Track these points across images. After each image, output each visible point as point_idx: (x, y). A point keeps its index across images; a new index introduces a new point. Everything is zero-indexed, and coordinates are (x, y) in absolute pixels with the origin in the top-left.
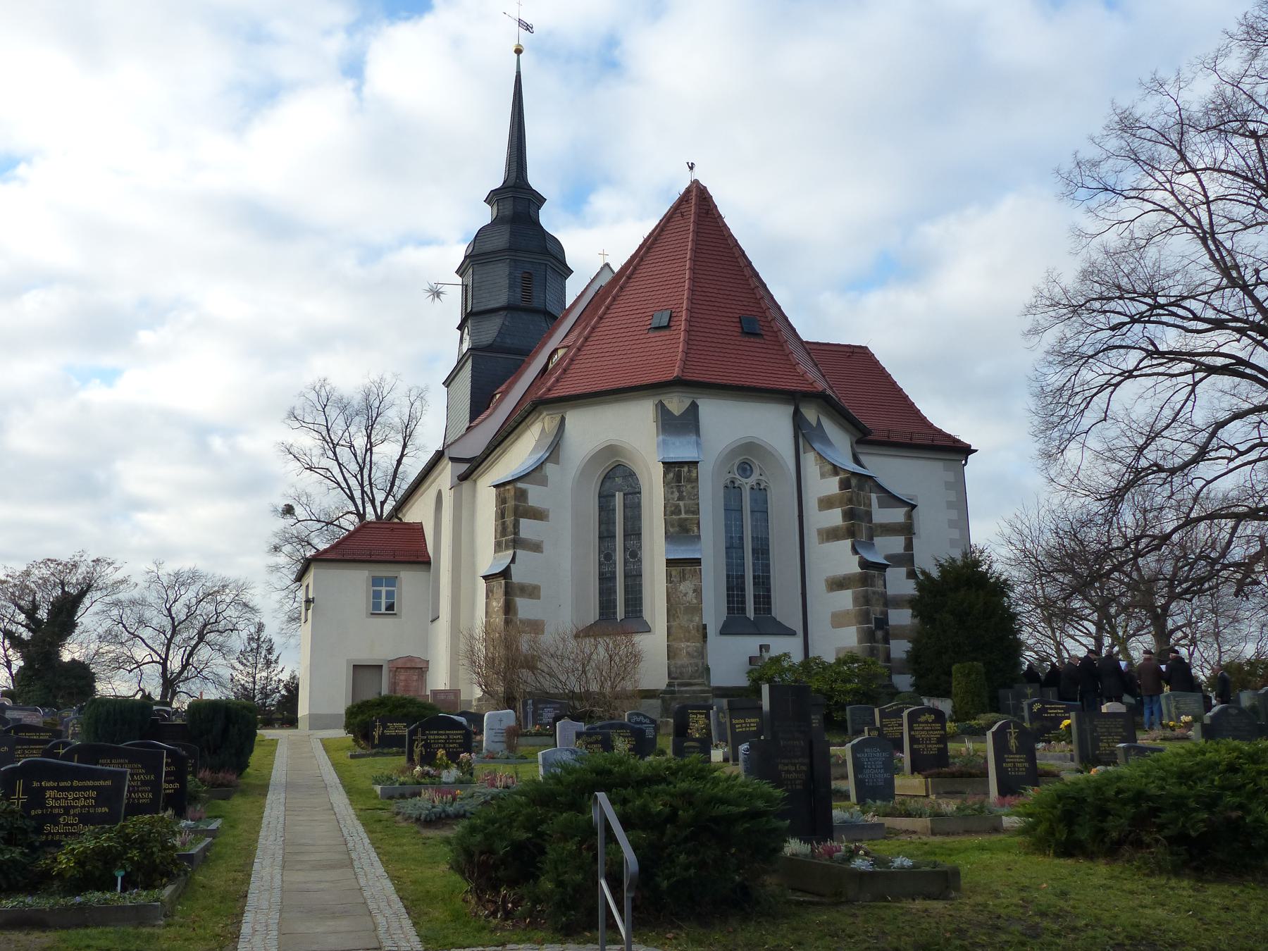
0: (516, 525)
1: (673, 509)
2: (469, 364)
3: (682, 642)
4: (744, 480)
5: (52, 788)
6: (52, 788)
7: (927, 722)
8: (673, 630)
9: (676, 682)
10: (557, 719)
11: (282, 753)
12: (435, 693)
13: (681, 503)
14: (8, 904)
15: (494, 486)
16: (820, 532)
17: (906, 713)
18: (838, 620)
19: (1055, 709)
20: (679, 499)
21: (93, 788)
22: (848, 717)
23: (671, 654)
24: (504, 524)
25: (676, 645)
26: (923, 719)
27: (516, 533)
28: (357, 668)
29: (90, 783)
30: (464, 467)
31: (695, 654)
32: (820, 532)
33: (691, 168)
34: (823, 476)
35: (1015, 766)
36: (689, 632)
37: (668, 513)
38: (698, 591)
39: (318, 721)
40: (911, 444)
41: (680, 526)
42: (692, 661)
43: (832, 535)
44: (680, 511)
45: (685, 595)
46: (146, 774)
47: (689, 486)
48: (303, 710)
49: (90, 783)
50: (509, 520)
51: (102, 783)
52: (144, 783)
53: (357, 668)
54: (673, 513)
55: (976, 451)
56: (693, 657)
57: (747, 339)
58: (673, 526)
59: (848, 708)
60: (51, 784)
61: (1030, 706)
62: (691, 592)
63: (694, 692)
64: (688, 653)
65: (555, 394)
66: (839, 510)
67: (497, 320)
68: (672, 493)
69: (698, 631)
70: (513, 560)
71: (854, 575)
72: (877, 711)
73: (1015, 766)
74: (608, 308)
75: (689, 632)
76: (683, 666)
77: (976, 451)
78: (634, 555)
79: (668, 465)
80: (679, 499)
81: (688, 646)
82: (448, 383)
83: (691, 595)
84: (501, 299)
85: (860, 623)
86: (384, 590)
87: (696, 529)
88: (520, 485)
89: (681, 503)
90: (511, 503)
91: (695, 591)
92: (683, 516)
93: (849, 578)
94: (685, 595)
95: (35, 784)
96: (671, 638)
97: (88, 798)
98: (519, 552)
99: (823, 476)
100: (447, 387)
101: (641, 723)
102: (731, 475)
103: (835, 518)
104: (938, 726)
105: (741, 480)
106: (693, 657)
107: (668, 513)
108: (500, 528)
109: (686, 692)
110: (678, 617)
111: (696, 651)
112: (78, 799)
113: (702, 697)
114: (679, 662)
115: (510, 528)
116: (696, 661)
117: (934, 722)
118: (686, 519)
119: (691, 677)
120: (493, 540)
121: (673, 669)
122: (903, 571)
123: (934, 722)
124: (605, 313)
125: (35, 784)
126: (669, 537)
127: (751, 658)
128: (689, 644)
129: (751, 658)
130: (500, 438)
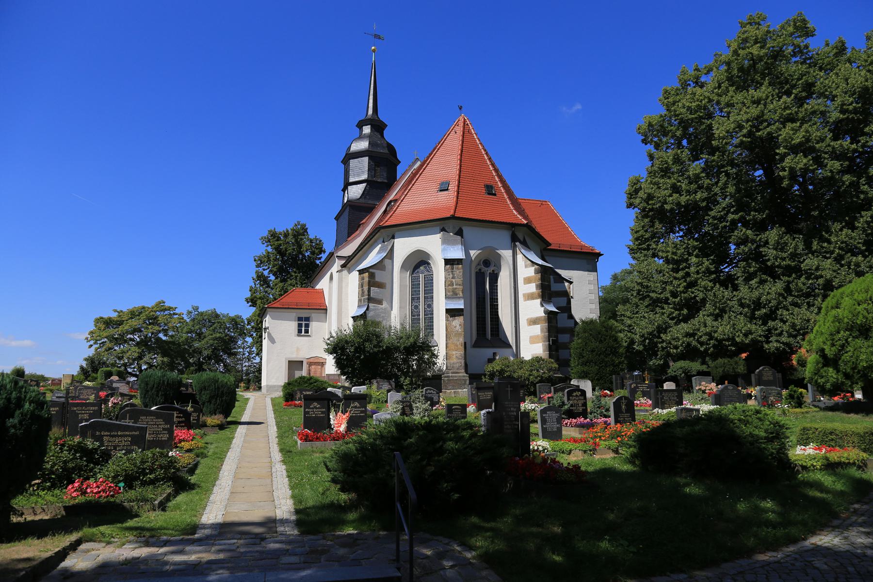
0: (369, 291)
2: (347, 210)
4: (486, 269)
5: (107, 436)
6: (107, 436)
7: (577, 396)
8: (449, 345)
9: (450, 371)
10: (389, 391)
11: (250, 404)
12: (328, 375)
14: (859, 538)
17: (566, 390)
18: (533, 340)
19: (643, 386)
20: (453, 278)
21: (129, 436)
23: (448, 358)
24: (363, 290)
25: (450, 352)
26: (574, 394)
27: (369, 295)
28: (289, 362)
29: (127, 433)
32: (524, 295)
33: (460, 109)
34: (526, 266)
35: (624, 420)
37: (447, 285)
39: (270, 388)
40: (559, 250)
42: (458, 361)
43: (530, 297)
45: (455, 327)
46: (166, 424)
47: (458, 271)
48: (264, 383)
49: (127, 433)
50: (366, 288)
51: (134, 433)
52: (164, 429)
53: (289, 362)
54: (449, 285)
55: (603, 255)
57: (488, 196)
58: (449, 292)
59: (537, 385)
60: (106, 433)
61: (631, 385)
63: (460, 376)
65: (387, 224)
66: (541, 344)
68: (449, 275)
70: (367, 309)
72: (552, 388)
73: (624, 420)
76: (454, 363)
77: (603, 255)
78: (429, 307)
79: (448, 262)
80: (453, 278)
81: (457, 354)
82: (337, 218)
84: (365, 176)
85: (544, 342)
86: (304, 323)
88: (371, 270)
89: (454, 280)
90: (366, 279)
92: (455, 287)
94: (455, 327)
95: (98, 433)
96: (448, 349)
97: (126, 441)
98: (370, 305)
99: (526, 266)
100: (337, 220)
101: (431, 393)
102: (479, 267)
103: (532, 288)
104: (582, 398)
105: (484, 269)
106: (459, 359)
107: (447, 285)
108: (361, 292)
109: (456, 377)
112: (121, 441)
114: (452, 362)
115: (366, 293)
116: (460, 361)
117: (580, 395)
119: (458, 369)
120: (357, 299)
121: (449, 365)
122: (566, 315)
123: (580, 395)
125: (98, 433)
126: (447, 297)
127: (488, 359)
129: (488, 359)
130: (362, 246)
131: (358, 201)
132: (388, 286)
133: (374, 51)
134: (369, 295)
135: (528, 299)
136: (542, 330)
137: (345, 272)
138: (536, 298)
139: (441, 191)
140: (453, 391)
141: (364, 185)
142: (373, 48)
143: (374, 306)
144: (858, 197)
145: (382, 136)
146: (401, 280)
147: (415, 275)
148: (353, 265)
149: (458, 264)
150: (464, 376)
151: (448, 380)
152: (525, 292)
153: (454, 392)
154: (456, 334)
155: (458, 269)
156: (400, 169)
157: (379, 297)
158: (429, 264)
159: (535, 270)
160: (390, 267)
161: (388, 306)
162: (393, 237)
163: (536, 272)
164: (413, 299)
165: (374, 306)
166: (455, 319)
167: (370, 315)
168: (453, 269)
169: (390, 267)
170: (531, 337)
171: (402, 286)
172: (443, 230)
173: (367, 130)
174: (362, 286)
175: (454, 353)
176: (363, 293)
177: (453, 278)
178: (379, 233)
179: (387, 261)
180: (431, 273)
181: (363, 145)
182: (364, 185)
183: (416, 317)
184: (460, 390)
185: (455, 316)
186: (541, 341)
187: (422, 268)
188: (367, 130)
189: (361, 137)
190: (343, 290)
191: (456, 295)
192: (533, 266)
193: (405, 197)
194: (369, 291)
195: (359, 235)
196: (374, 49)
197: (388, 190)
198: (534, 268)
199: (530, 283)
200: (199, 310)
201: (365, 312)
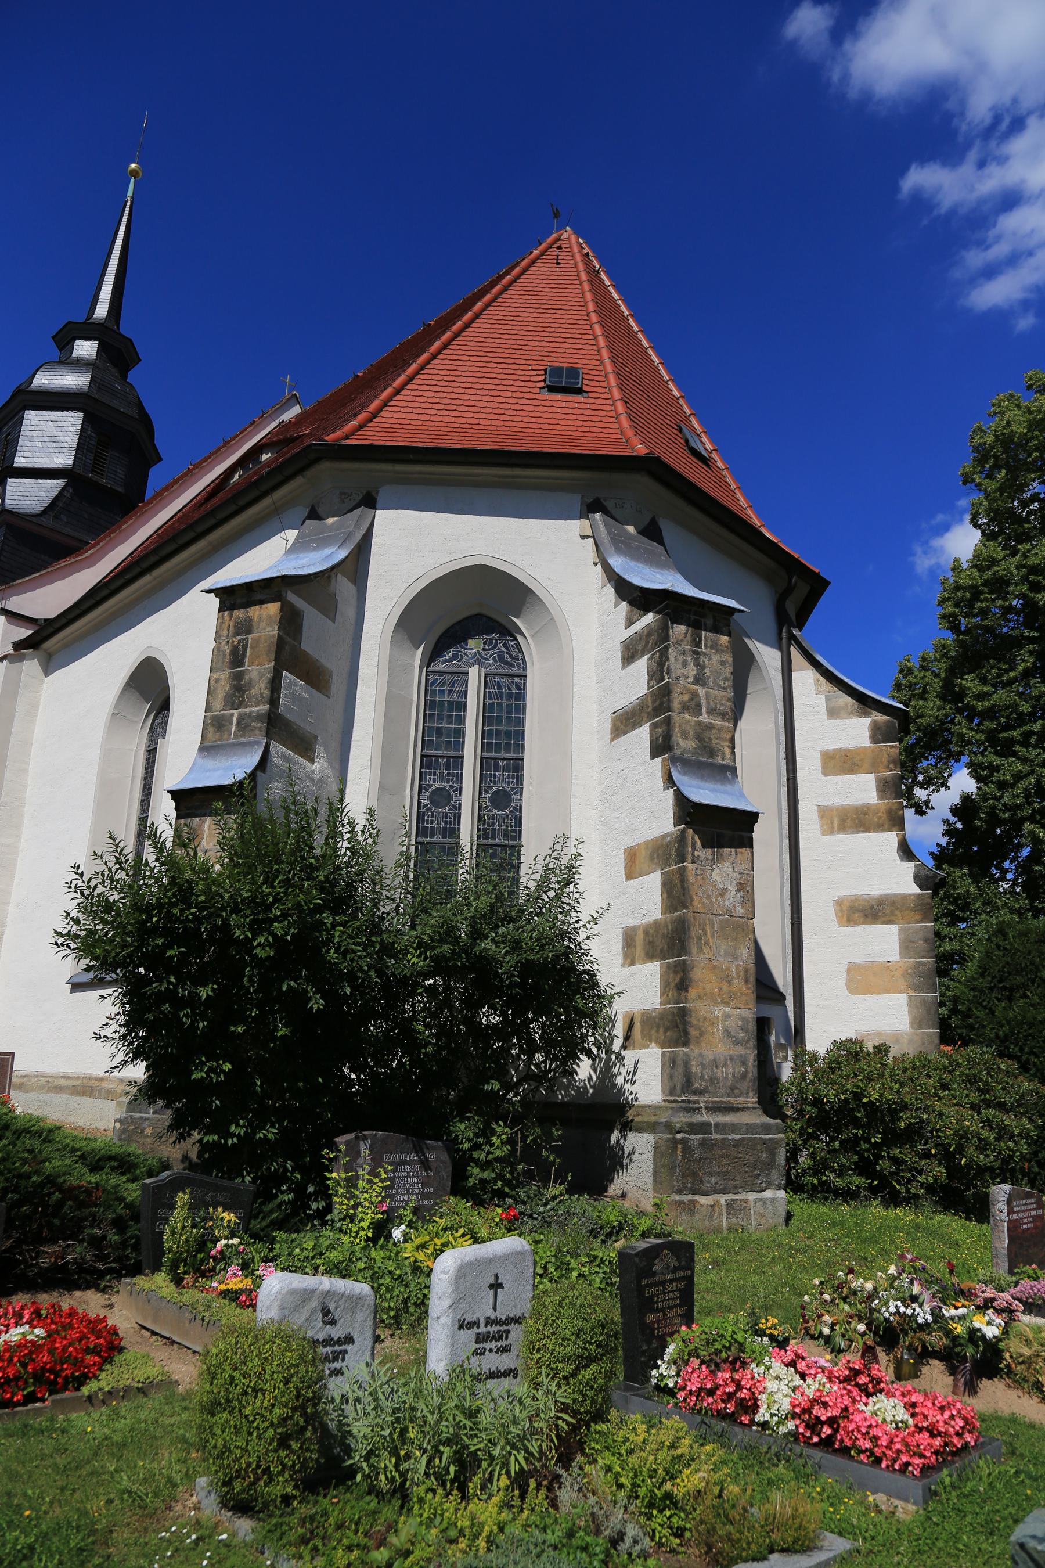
1: (686, 698)
3: (715, 1003)
9: (702, 1101)
13: (701, 691)
15: (579, 391)
16: (824, 813)
22: (768, 1194)
24: (238, 677)
27: (274, 701)
30: (24, 633)
31: (742, 1035)
32: (824, 813)
36: (729, 982)
38: (746, 888)
41: (699, 738)
44: (699, 705)
45: (723, 892)
47: (716, 658)
56: (737, 1042)
62: (733, 889)
64: (726, 1031)
67: (23, 460)
69: (747, 981)
70: (263, 763)
71: (905, 897)
74: (422, 368)
75: (729, 982)
76: (715, 1063)
81: (727, 1016)
83: (733, 895)
84: (64, 459)
87: (727, 751)
89: (701, 691)
91: (741, 887)
92: (705, 718)
93: (893, 903)
108: (224, 688)
109: (734, 1128)
110: (707, 943)
111: (742, 1029)
113: (764, 1142)
115: (260, 687)
116: (740, 1050)
118: (710, 727)
124: (439, 352)
128: (728, 1009)
131: (34, 520)
132: (338, 686)
133: (134, 173)
134: (274, 701)
135: (843, 828)
136: (906, 945)
137: (31, 666)
138: (880, 828)
139: (552, 389)
140: (723, 1199)
141: (57, 484)
142: (133, 166)
143: (286, 758)
144: (925, 772)
145: (124, 376)
146: (395, 672)
147: (441, 667)
148: (67, 646)
149: (716, 630)
150: (766, 1129)
151: (703, 1143)
152: (825, 802)
153: (730, 1205)
154: (724, 926)
155: (715, 646)
156: (156, 477)
157: (307, 724)
158: (509, 632)
159: (875, 729)
160: (351, 612)
161: (329, 772)
162: (370, 502)
163: (878, 734)
164: (427, 762)
165: (286, 758)
166: (720, 859)
167: (275, 789)
168: (698, 644)
169: (351, 612)
170: (853, 969)
171: (393, 701)
172: (591, 507)
173: (86, 349)
174: (237, 658)
175: (718, 1011)
176: (238, 691)
177: (699, 680)
178: (298, 481)
179: (343, 586)
180: (515, 671)
181: (74, 381)
182: (57, 484)
183: (438, 838)
184: (752, 1196)
185: (721, 846)
186: (902, 983)
187: (474, 644)
188: (86, 349)
189: (66, 362)
190: (16, 728)
191: (712, 753)
192: (865, 714)
193: (407, 383)
194: (275, 684)
195: (91, 562)
196: (133, 170)
197: (122, 517)
198: (867, 721)
199: (851, 771)
200: (142, 1380)
201: (252, 776)
